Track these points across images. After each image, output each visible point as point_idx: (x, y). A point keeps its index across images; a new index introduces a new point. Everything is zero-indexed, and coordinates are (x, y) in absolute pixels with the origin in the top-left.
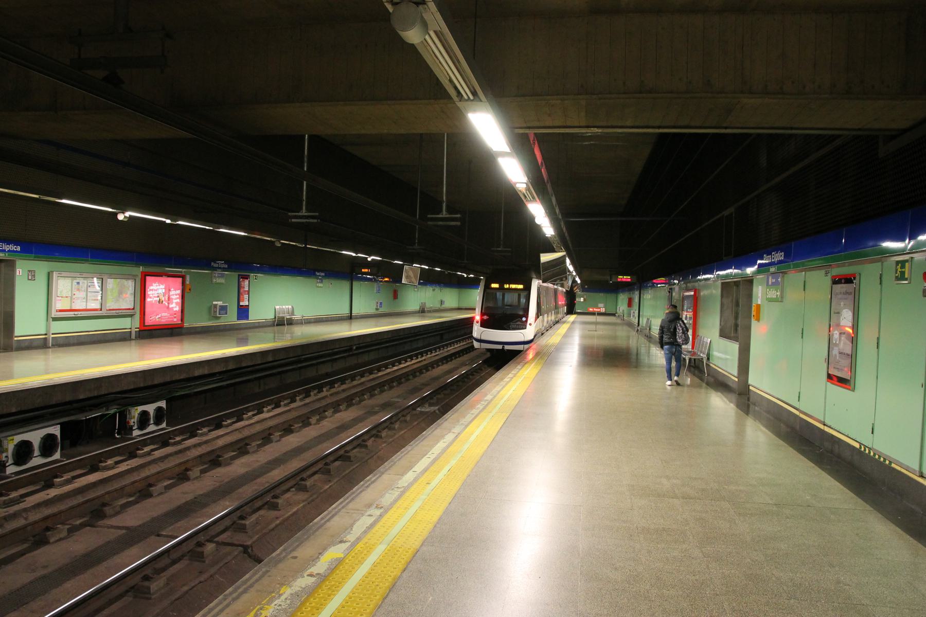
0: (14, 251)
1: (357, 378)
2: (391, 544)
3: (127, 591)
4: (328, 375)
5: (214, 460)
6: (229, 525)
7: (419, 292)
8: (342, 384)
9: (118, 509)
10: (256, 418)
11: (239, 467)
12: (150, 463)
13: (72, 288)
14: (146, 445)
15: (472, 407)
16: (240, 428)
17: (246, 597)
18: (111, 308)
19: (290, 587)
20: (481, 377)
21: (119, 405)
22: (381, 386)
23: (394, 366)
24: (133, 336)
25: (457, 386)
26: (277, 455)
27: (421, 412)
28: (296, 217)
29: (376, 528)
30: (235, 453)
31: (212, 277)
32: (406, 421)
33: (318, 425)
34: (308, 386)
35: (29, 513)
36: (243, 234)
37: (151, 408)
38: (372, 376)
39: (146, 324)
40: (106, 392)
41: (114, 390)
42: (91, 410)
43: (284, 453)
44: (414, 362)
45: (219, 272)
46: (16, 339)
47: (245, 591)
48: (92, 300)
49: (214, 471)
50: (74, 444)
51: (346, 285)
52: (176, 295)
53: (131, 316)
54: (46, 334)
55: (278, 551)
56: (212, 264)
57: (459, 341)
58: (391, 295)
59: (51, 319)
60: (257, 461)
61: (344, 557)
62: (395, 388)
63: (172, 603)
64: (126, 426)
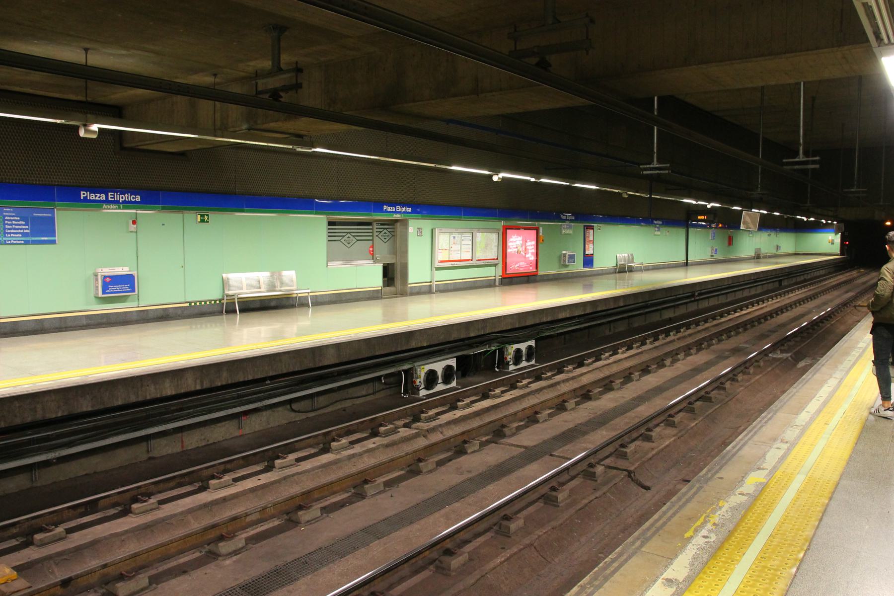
0: (131, 202)
1: (701, 324)
2: (809, 475)
3: (539, 498)
4: (671, 321)
5: (585, 395)
6: (613, 451)
7: (754, 239)
8: (687, 329)
9: (514, 430)
10: (613, 359)
11: (607, 402)
12: (529, 394)
13: (450, 242)
14: (524, 379)
15: (847, 353)
16: (600, 367)
17: (690, 506)
18: (480, 259)
19: (727, 502)
20: (832, 325)
21: (499, 343)
22: (728, 331)
23: (735, 312)
24: (497, 284)
25: (808, 333)
26: (640, 393)
27: (774, 359)
28: (646, 169)
29: (789, 459)
30: (601, 389)
31: (561, 229)
32: (759, 366)
33: (671, 367)
34: (657, 329)
35: (443, 428)
36: (594, 187)
37: (523, 346)
38: (715, 322)
39: (507, 272)
40: (490, 332)
41: (496, 330)
42: (477, 347)
43: (646, 392)
44: (755, 308)
45: (567, 223)
46: (409, 286)
47: (688, 501)
48: (465, 252)
49: (586, 404)
50: (464, 375)
51: (682, 232)
52: (531, 245)
53: (495, 265)
54: (431, 282)
55: (704, 471)
56: (562, 216)
57: (801, 288)
58: (726, 242)
59: (435, 269)
60: (623, 397)
61: (768, 482)
62: (741, 334)
63: (576, 512)
64: (504, 361)
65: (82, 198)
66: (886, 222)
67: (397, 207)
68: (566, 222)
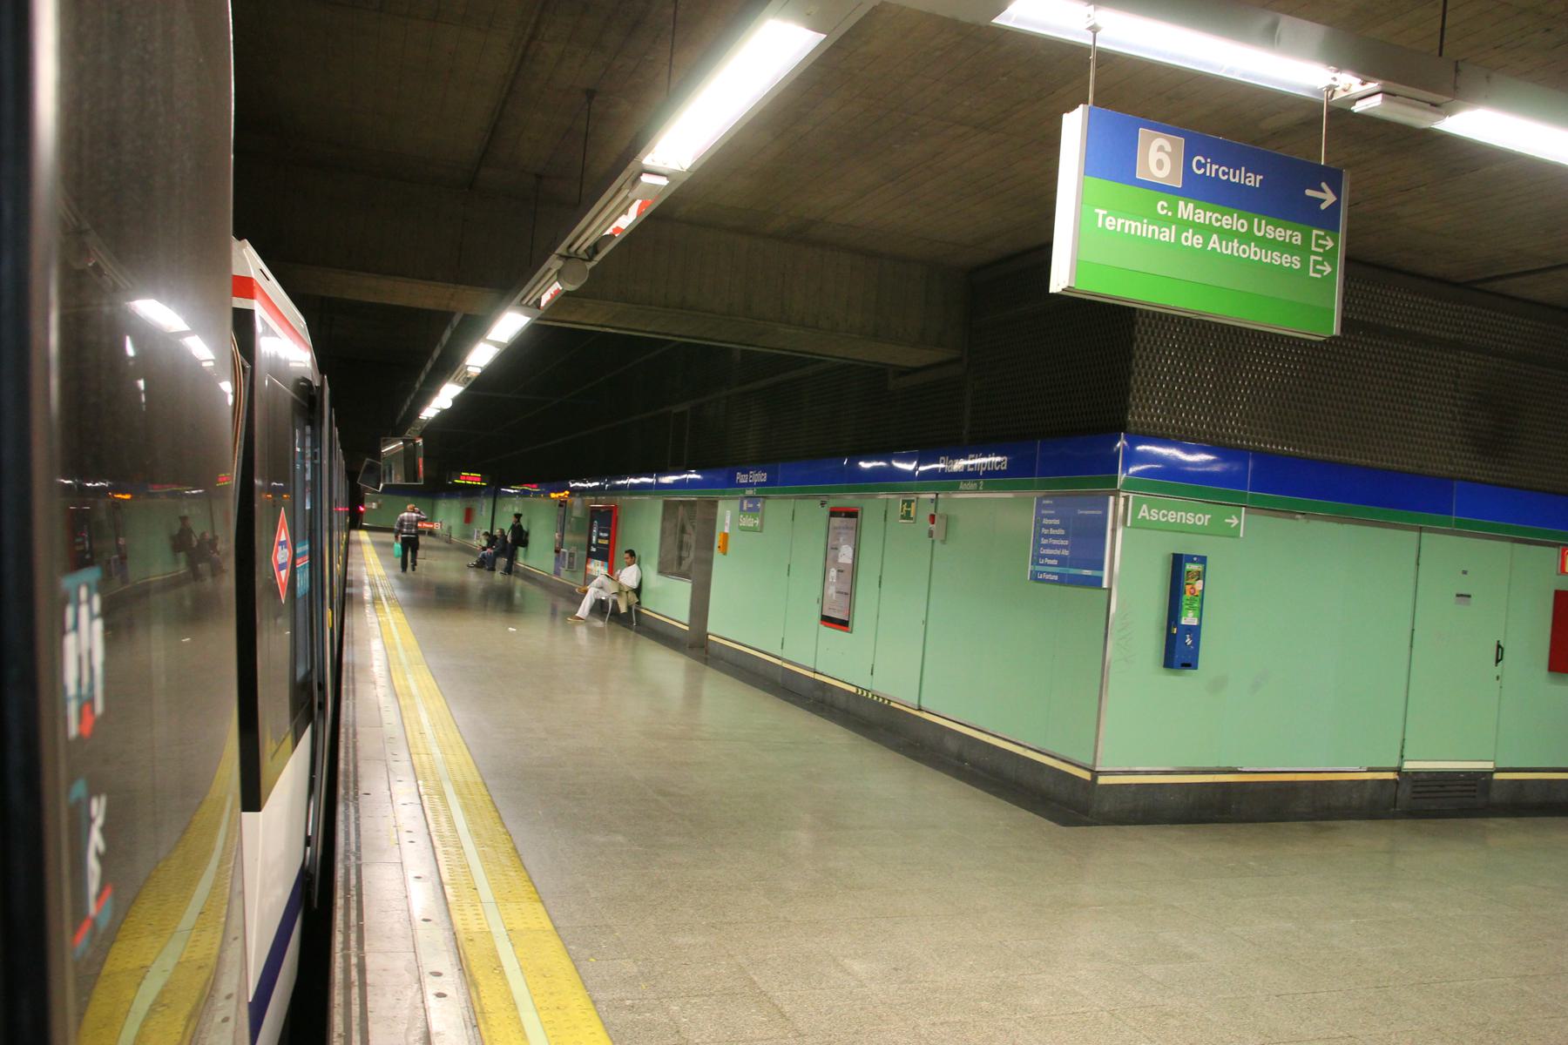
65: (1139, 517)
66: (861, 461)
68: (962, 486)
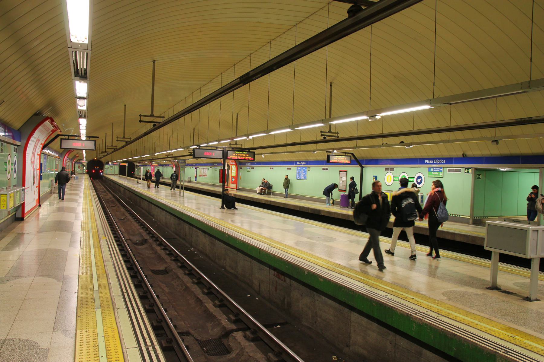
67: (434, 160)
